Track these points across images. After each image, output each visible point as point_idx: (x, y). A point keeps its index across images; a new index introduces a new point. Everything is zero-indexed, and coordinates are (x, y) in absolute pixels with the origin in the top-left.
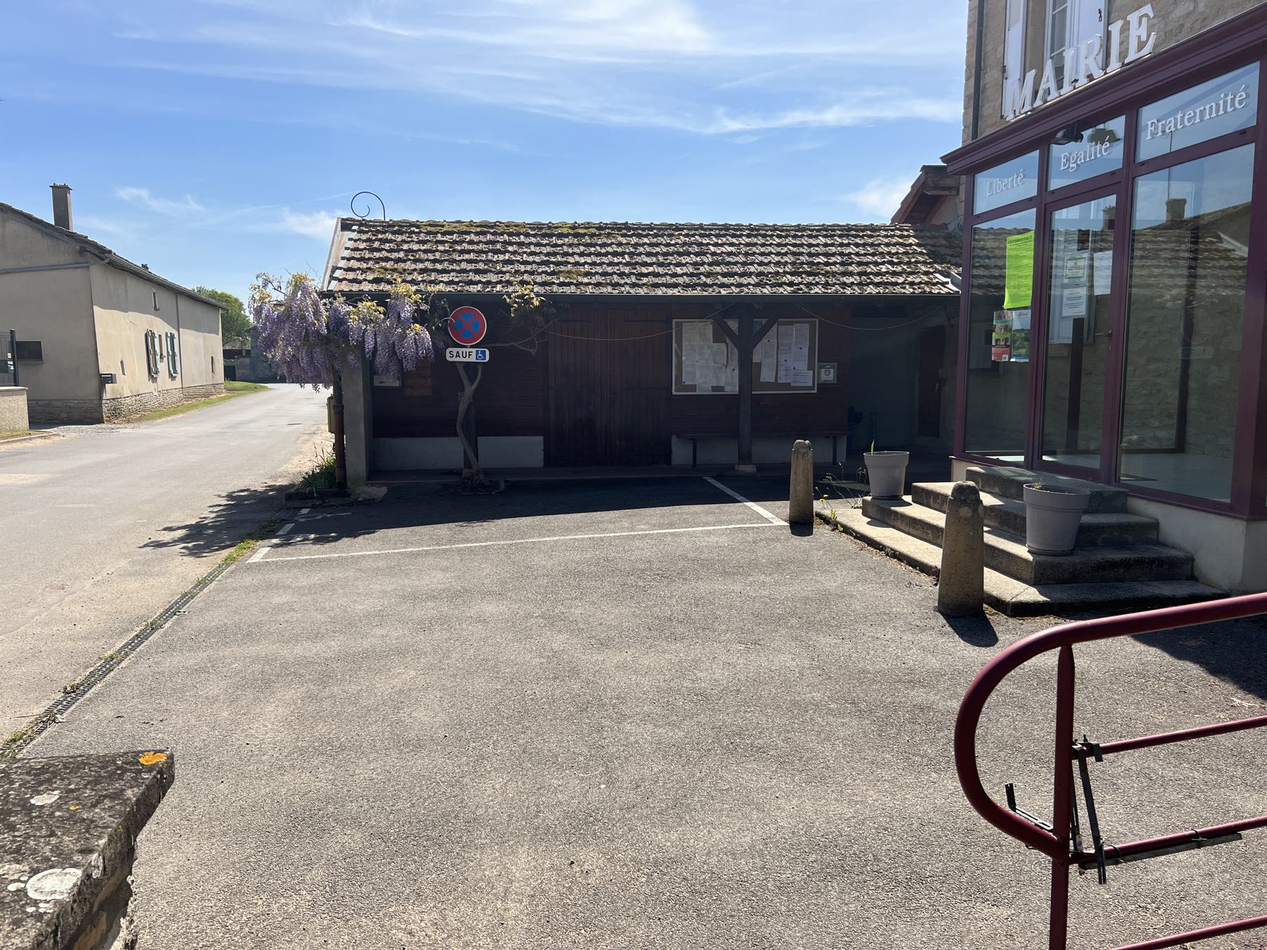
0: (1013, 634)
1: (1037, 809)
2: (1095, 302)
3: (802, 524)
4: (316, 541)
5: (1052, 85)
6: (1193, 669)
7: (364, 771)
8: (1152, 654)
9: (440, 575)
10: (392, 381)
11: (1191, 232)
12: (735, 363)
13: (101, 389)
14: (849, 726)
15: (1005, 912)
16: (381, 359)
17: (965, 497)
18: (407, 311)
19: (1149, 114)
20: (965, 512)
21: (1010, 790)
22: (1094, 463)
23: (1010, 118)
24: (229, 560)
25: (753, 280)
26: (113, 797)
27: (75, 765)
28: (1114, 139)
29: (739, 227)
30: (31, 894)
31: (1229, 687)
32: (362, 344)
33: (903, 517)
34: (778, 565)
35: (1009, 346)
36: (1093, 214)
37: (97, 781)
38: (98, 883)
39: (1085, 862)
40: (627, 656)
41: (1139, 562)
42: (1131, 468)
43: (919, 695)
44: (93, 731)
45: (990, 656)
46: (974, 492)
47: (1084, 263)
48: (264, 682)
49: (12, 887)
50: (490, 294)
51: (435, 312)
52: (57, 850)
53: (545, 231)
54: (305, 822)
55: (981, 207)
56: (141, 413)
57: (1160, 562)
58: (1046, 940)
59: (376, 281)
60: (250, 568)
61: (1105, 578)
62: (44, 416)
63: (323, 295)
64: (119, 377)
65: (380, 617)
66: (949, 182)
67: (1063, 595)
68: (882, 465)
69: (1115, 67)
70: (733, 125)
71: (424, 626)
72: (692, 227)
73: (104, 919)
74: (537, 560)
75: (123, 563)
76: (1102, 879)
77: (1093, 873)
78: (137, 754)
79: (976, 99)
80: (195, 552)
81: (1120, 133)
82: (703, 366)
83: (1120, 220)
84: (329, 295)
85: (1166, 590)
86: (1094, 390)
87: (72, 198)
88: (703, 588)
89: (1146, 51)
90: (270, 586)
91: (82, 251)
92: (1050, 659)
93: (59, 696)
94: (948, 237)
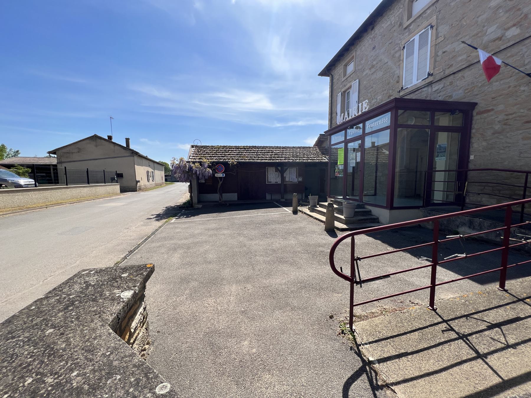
0: (340, 235)
1: (347, 272)
2: (357, 163)
3: (295, 212)
4: (186, 217)
5: (347, 117)
6: (379, 242)
7: (197, 269)
8: (371, 239)
9: (214, 225)
10: (203, 181)
11: (377, 148)
12: (280, 177)
13: (137, 184)
14: (305, 256)
15: (340, 295)
16: (201, 176)
17: (330, 205)
18: (206, 165)
19: (368, 123)
20: (330, 209)
21: (341, 268)
22: (357, 198)
23: (338, 124)
24: (166, 222)
25: (284, 158)
26: (140, 274)
27: (132, 267)
28: (360, 128)
29: (280, 147)
30: (122, 297)
31: (387, 246)
32: (196, 173)
33: (317, 210)
34: (290, 221)
35: (339, 173)
36: (356, 145)
37: (137, 271)
38: (137, 294)
39: (358, 283)
40: (257, 242)
41: (367, 219)
42: (365, 199)
43: (321, 249)
44: (135, 260)
45: (336, 240)
46: (332, 204)
47: (355, 155)
48: (175, 249)
49: (117, 295)
50: (225, 162)
51: (213, 165)
52: (128, 287)
53: (237, 148)
54: (185, 280)
55: (332, 143)
56: (146, 189)
57: (372, 219)
58: (349, 301)
59: (199, 159)
60: (171, 223)
61: (361, 221)
62: (123, 190)
63: (187, 162)
64: (141, 181)
65: (201, 234)
66: (325, 137)
67: (352, 227)
68: (312, 199)
69: (360, 113)
70: (278, 125)
71: (211, 236)
72: (270, 147)
73: (138, 302)
74: (236, 221)
75: (142, 223)
76: (361, 287)
77: (359, 286)
78: (146, 265)
79: (331, 120)
80: (157, 220)
81: (362, 127)
82: (273, 177)
83: (362, 146)
84: (189, 162)
85: (372, 225)
86: (357, 182)
87: (130, 141)
88: (274, 227)
89: (367, 110)
90: (176, 228)
91: (133, 153)
92: (349, 240)
93: (128, 253)
94: (325, 149)
